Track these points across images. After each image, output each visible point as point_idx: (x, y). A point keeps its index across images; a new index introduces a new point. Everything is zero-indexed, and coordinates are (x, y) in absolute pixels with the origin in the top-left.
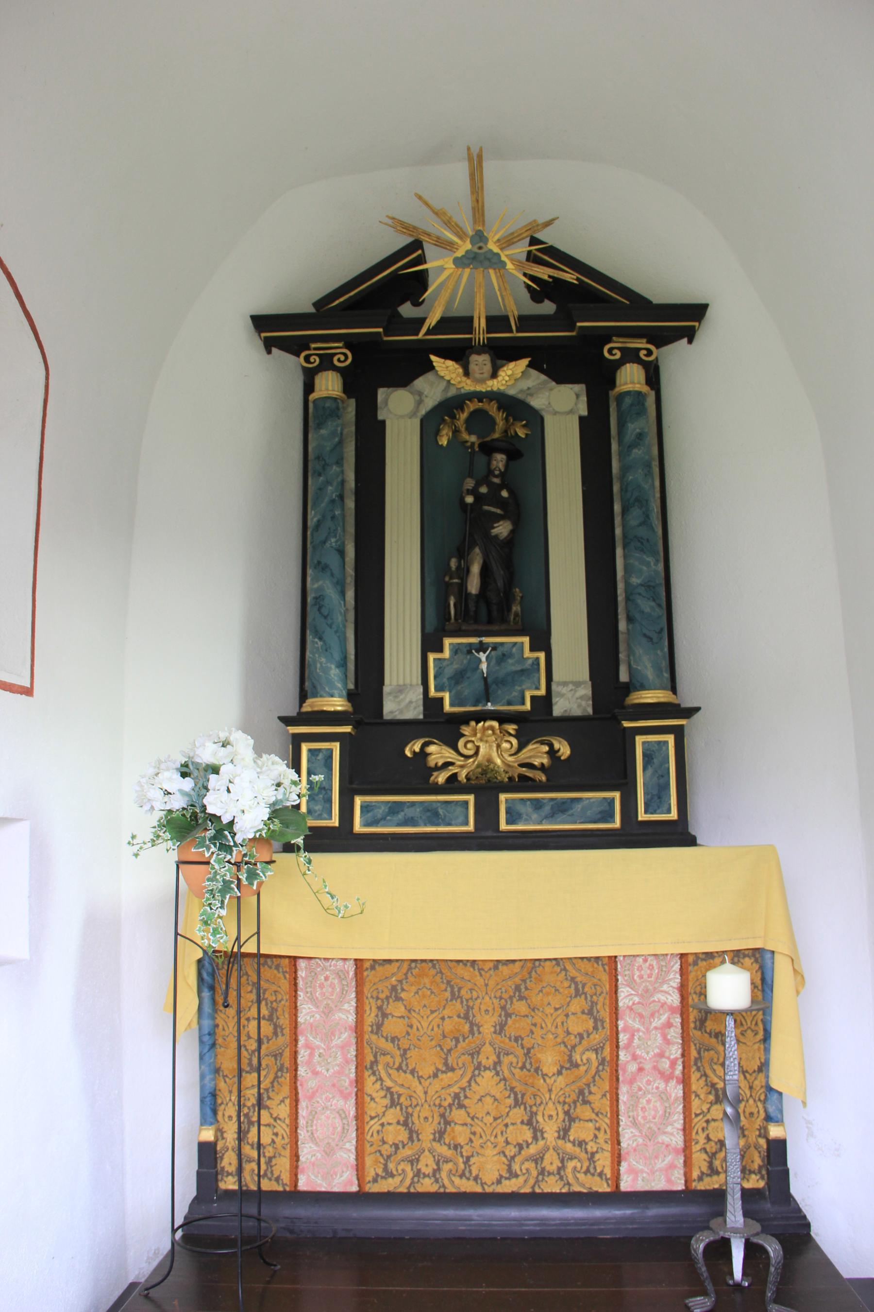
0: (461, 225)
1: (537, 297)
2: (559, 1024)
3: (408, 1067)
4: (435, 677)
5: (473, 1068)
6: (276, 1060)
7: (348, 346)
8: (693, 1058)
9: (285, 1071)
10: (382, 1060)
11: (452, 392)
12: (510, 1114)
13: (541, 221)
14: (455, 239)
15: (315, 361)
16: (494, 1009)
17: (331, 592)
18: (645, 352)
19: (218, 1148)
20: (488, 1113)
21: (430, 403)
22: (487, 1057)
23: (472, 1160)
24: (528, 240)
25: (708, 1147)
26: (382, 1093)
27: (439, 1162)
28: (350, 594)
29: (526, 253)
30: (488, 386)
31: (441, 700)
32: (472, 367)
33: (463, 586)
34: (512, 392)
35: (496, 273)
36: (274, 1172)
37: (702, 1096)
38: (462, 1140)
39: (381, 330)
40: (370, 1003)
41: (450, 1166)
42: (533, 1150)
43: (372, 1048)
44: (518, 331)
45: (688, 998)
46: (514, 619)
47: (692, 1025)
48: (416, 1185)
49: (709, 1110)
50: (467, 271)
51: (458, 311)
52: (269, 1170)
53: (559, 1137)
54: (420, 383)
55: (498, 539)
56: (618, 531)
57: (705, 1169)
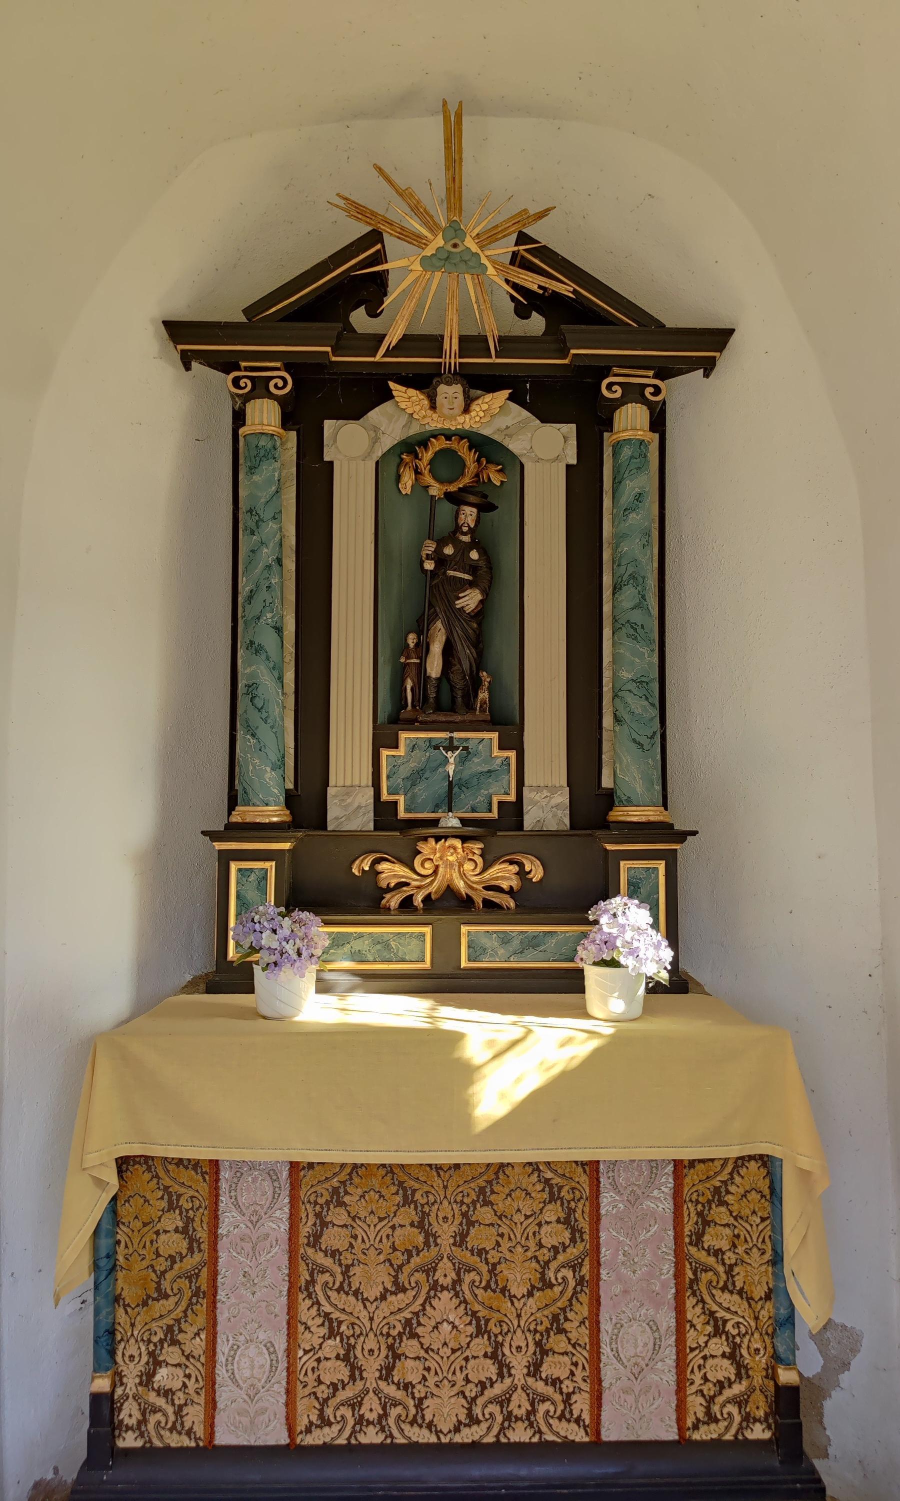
0: (432, 212)
1: (522, 312)
2: (531, 1234)
3: (351, 1287)
4: (388, 777)
5: (428, 1288)
6: (191, 1282)
7: (288, 368)
8: (687, 1280)
9: (202, 1296)
10: (321, 1279)
11: (414, 430)
12: (472, 1345)
13: (533, 210)
14: (424, 231)
15: (246, 386)
16: (454, 1216)
17: (267, 681)
18: (651, 390)
19: (116, 1397)
20: (445, 1344)
21: (387, 443)
22: (445, 1273)
23: (426, 1403)
24: (515, 236)
25: (705, 1389)
26: (319, 1321)
27: (387, 1404)
28: (290, 676)
29: (511, 253)
30: (459, 424)
31: (395, 804)
32: (440, 399)
33: (421, 668)
34: (486, 432)
35: (473, 279)
36: (185, 1424)
37: (699, 1327)
38: (414, 1378)
39: (329, 349)
40: (306, 1209)
41: (399, 1410)
42: (498, 1389)
43: (307, 1265)
44: (497, 357)
45: (682, 1207)
46: (481, 706)
47: (687, 1240)
48: (358, 1435)
49: (706, 1343)
50: (438, 275)
51: (425, 328)
52: (179, 1421)
53: (528, 1374)
54: (375, 415)
55: (464, 611)
56: (607, 608)
57: (701, 1415)
